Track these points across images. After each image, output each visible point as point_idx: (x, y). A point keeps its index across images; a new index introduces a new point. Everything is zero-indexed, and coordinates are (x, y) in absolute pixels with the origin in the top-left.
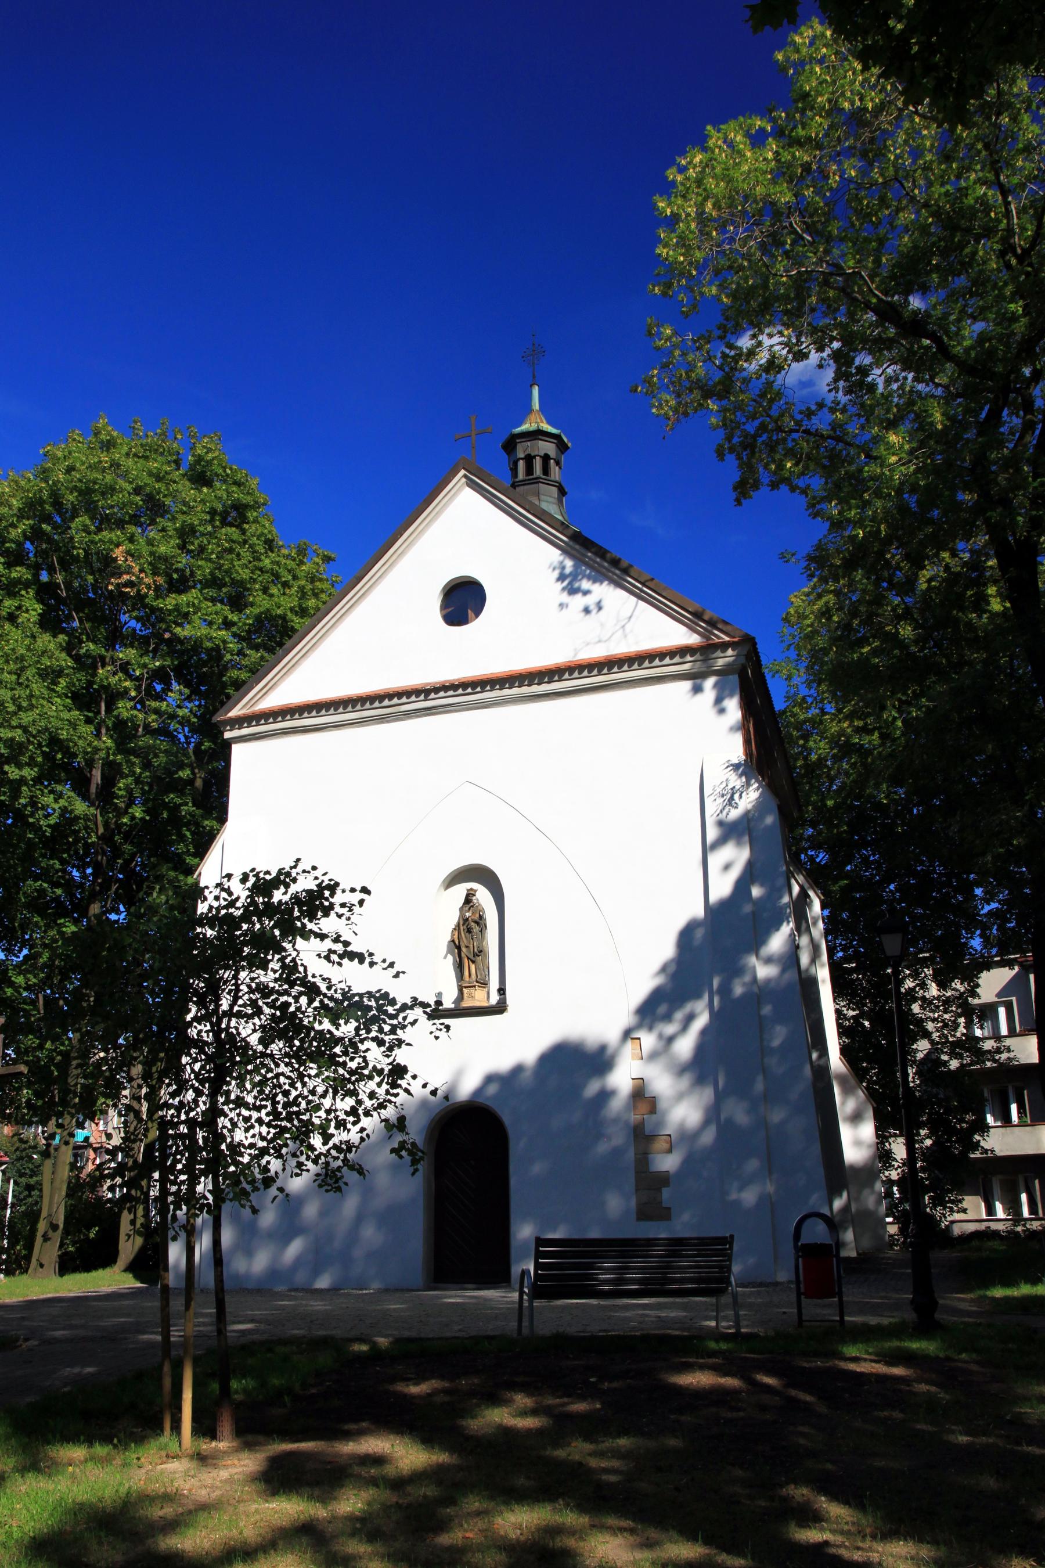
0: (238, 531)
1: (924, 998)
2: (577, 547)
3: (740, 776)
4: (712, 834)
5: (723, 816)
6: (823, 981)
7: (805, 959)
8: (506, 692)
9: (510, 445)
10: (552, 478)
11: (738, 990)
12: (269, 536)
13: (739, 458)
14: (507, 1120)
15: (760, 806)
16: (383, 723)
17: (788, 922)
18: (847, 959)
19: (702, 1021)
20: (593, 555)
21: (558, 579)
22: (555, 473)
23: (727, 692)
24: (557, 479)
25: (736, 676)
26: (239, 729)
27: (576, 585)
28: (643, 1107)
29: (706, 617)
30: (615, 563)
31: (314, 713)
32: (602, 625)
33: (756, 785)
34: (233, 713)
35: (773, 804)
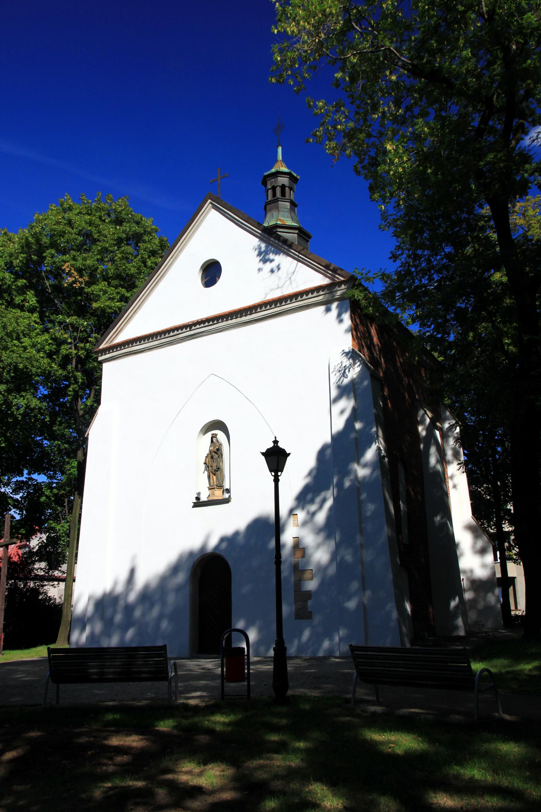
2: (266, 236)
3: (349, 359)
4: (334, 393)
5: (339, 383)
8: (230, 322)
9: (264, 183)
11: (347, 484)
12: (151, 249)
14: (230, 563)
15: (361, 375)
16: (171, 345)
17: (376, 443)
19: (329, 503)
20: (273, 240)
23: (344, 310)
26: (105, 355)
27: (267, 257)
28: (299, 554)
29: (331, 268)
31: (138, 343)
32: (280, 278)
34: (101, 347)
35: (368, 374)
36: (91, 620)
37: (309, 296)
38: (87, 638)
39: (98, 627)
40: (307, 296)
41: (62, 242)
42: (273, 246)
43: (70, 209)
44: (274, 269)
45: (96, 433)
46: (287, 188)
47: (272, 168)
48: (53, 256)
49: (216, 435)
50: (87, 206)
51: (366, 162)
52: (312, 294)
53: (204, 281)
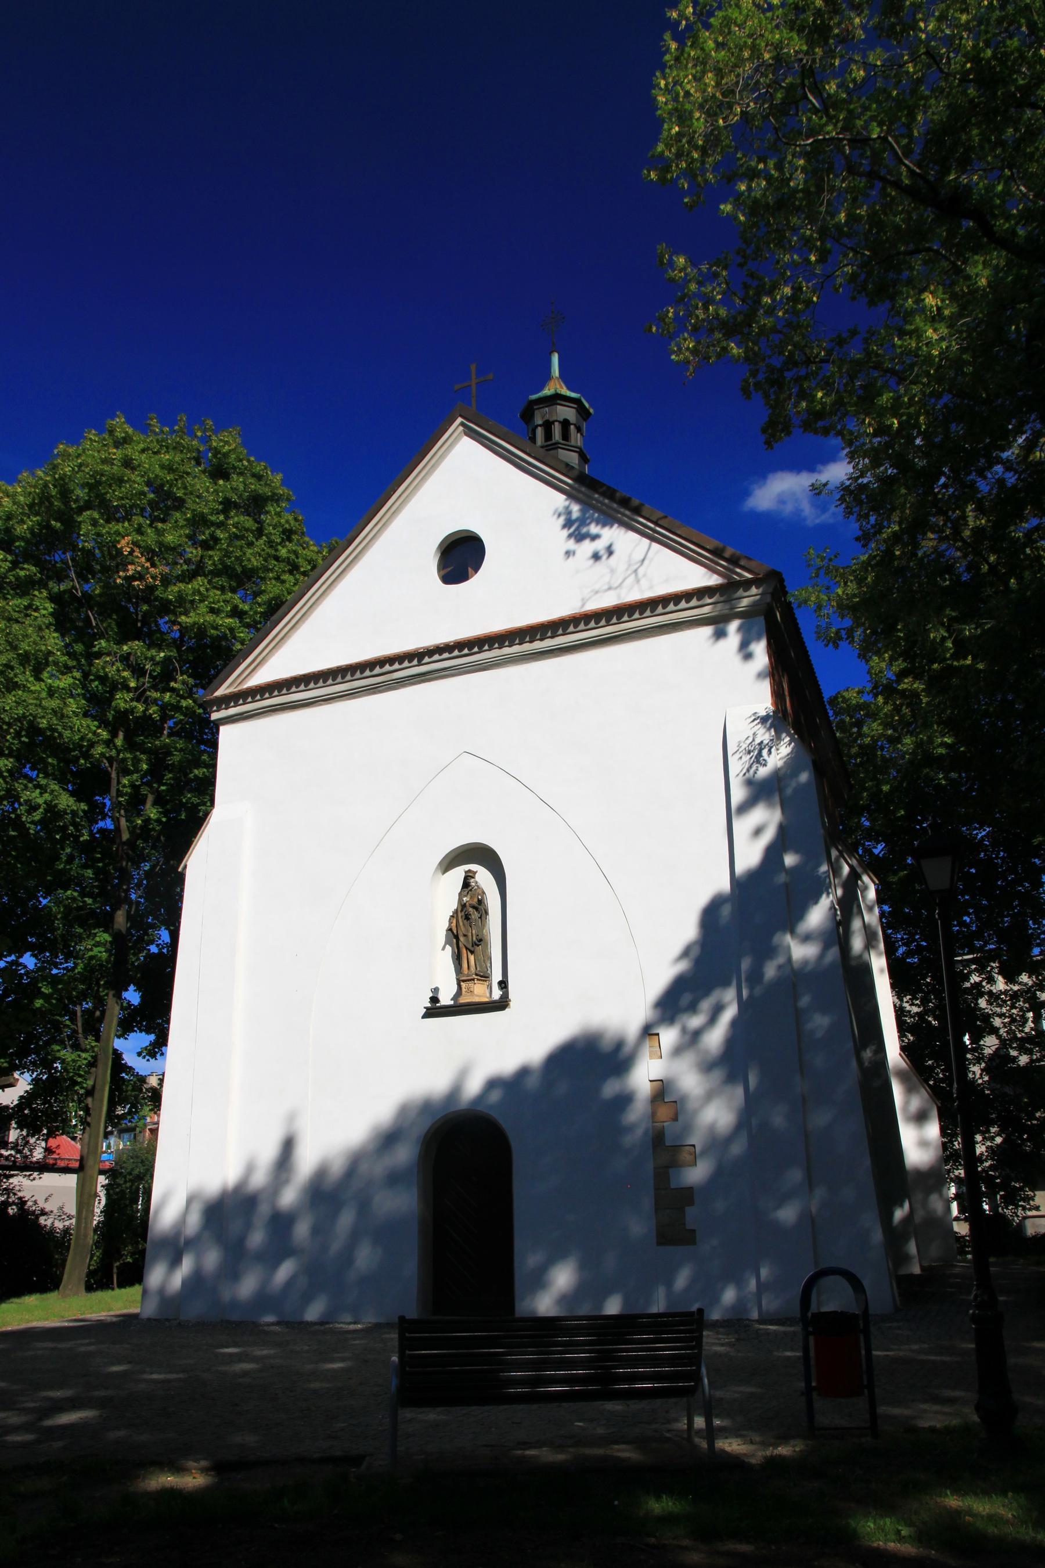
0: (250, 519)
1: (990, 993)
2: (583, 489)
3: (769, 729)
4: (738, 794)
6: (882, 971)
7: (857, 943)
8: (506, 650)
9: (527, 415)
10: (573, 443)
11: (770, 971)
12: (287, 526)
13: (767, 396)
15: (793, 765)
16: (374, 693)
17: (828, 894)
18: (909, 954)
19: (729, 1014)
20: (602, 493)
21: (564, 526)
22: (577, 439)
24: (579, 444)
25: (762, 618)
26: (226, 709)
27: (584, 530)
29: (727, 555)
30: (625, 503)
31: (302, 687)
32: (613, 571)
33: (788, 739)
34: (220, 692)
35: (807, 759)
36: (191, 1243)
37: (679, 607)
38: (184, 1283)
39: (212, 1258)
40: (676, 605)
41: (115, 496)
42: (596, 509)
43: (126, 440)
44: (601, 553)
45: (201, 865)
46: (572, 427)
47: (542, 389)
48: (94, 523)
49: (475, 873)
50: (160, 437)
51: (761, 377)
52: (687, 602)
53: (443, 573)
